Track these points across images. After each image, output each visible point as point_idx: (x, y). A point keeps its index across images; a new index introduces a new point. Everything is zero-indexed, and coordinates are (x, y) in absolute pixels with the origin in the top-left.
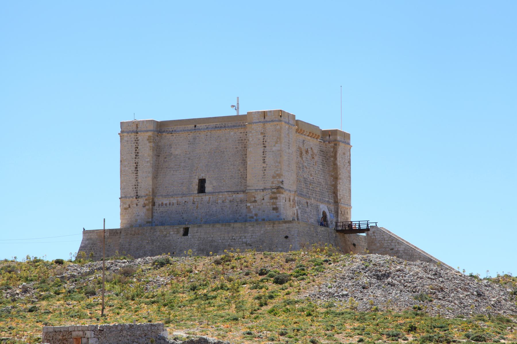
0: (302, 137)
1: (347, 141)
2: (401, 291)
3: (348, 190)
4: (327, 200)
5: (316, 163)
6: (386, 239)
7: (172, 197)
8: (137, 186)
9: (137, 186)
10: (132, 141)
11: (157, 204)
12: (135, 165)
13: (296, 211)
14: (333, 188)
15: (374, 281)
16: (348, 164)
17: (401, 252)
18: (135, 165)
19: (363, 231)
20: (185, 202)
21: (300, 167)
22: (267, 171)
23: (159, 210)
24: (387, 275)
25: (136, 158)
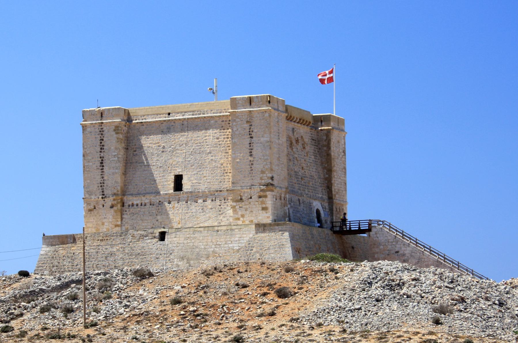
0: (292, 125)
1: (341, 127)
2: (419, 303)
3: (343, 184)
4: (320, 196)
5: (307, 153)
6: (390, 241)
7: (144, 196)
8: (102, 184)
9: (102, 184)
10: (96, 132)
11: (126, 205)
12: (100, 159)
13: (287, 211)
14: (326, 182)
15: (387, 292)
16: (343, 154)
17: (407, 255)
18: (100, 159)
19: (364, 231)
20: (160, 201)
21: (290, 160)
22: (254, 165)
23: (129, 211)
24: (401, 285)
25: (101, 152)
